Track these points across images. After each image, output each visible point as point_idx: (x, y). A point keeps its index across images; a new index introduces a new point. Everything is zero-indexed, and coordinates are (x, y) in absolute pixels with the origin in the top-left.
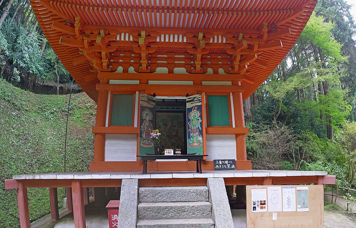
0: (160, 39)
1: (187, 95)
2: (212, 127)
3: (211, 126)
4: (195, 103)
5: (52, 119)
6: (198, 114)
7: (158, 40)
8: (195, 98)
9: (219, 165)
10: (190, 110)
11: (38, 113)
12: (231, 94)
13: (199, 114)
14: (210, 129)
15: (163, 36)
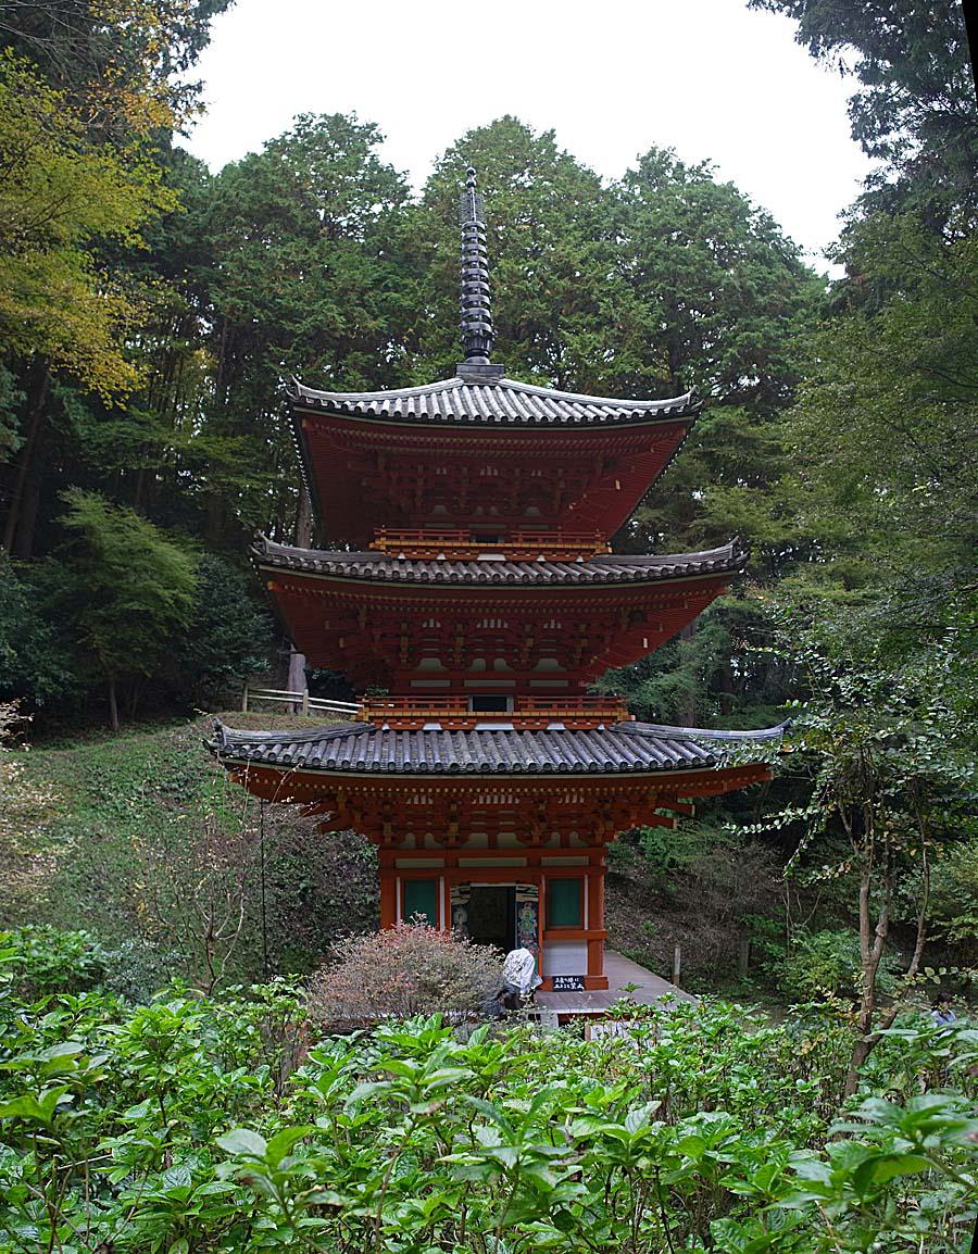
0: (486, 472)
1: (518, 882)
2: (554, 930)
3: (556, 927)
4: (529, 896)
5: (138, 816)
6: (532, 915)
7: (482, 473)
8: (529, 889)
9: (559, 984)
10: (522, 905)
11: (93, 807)
12: (586, 877)
13: (535, 915)
14: (549, 933)
15: (486, 621)
